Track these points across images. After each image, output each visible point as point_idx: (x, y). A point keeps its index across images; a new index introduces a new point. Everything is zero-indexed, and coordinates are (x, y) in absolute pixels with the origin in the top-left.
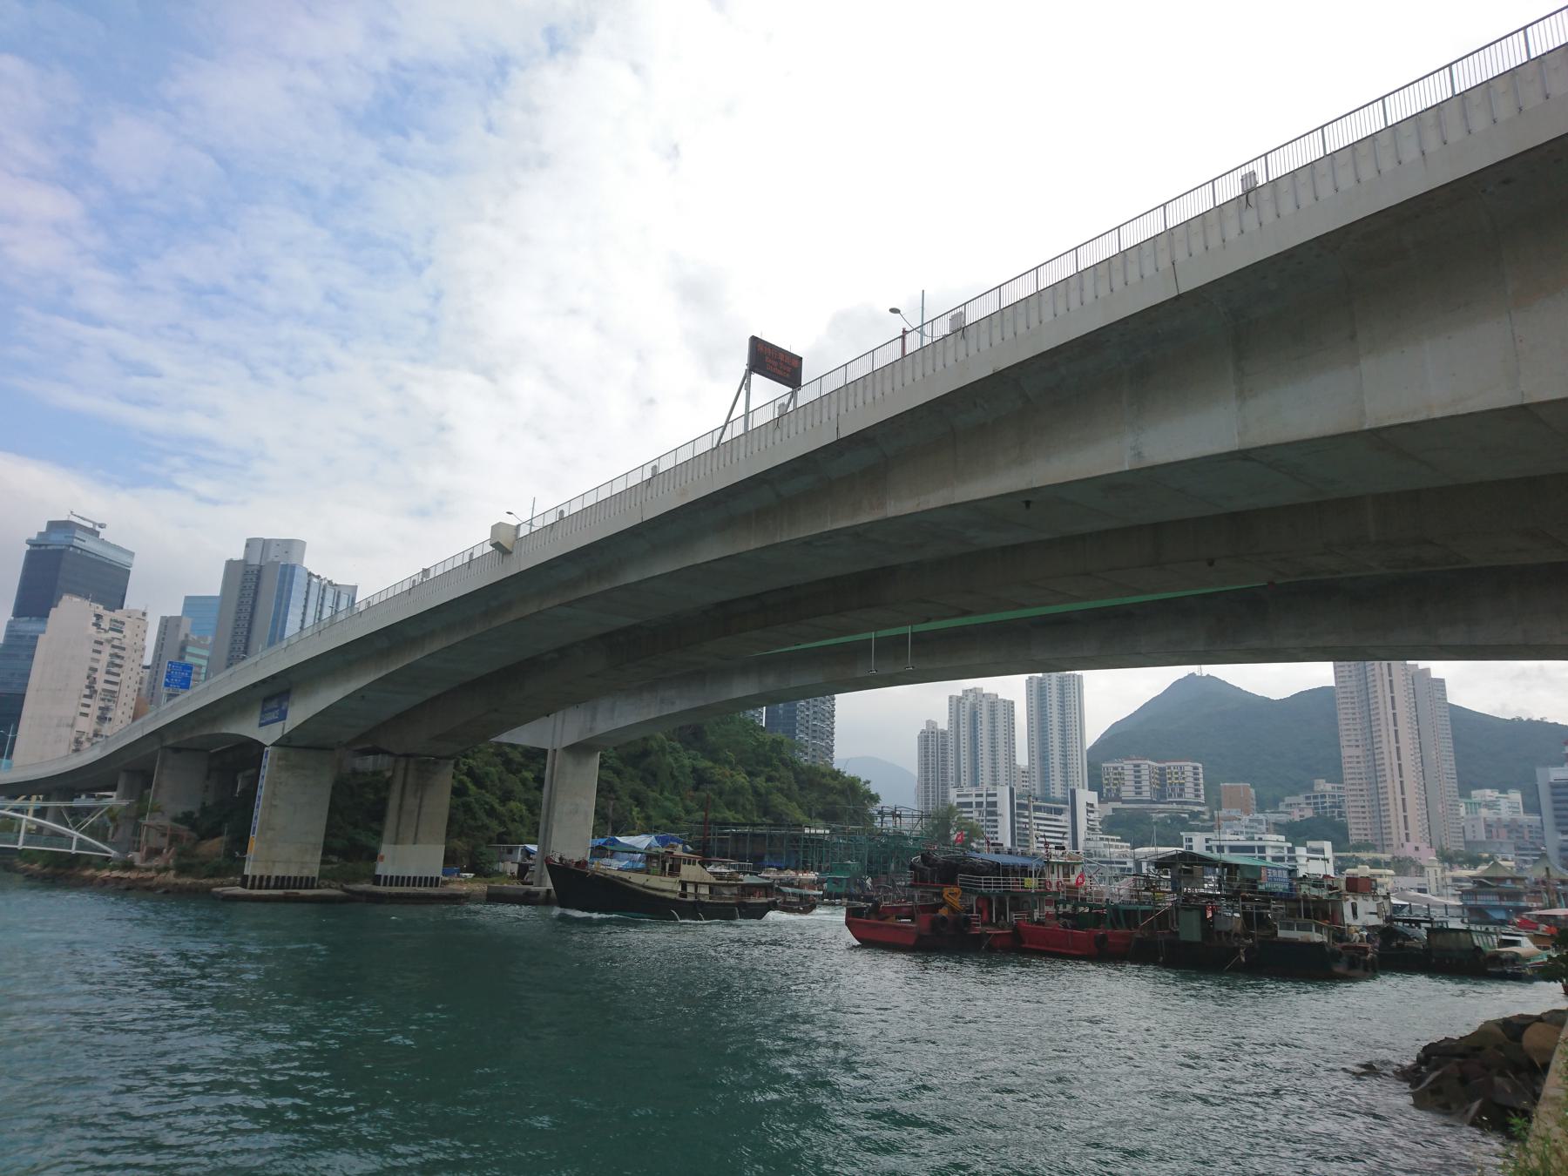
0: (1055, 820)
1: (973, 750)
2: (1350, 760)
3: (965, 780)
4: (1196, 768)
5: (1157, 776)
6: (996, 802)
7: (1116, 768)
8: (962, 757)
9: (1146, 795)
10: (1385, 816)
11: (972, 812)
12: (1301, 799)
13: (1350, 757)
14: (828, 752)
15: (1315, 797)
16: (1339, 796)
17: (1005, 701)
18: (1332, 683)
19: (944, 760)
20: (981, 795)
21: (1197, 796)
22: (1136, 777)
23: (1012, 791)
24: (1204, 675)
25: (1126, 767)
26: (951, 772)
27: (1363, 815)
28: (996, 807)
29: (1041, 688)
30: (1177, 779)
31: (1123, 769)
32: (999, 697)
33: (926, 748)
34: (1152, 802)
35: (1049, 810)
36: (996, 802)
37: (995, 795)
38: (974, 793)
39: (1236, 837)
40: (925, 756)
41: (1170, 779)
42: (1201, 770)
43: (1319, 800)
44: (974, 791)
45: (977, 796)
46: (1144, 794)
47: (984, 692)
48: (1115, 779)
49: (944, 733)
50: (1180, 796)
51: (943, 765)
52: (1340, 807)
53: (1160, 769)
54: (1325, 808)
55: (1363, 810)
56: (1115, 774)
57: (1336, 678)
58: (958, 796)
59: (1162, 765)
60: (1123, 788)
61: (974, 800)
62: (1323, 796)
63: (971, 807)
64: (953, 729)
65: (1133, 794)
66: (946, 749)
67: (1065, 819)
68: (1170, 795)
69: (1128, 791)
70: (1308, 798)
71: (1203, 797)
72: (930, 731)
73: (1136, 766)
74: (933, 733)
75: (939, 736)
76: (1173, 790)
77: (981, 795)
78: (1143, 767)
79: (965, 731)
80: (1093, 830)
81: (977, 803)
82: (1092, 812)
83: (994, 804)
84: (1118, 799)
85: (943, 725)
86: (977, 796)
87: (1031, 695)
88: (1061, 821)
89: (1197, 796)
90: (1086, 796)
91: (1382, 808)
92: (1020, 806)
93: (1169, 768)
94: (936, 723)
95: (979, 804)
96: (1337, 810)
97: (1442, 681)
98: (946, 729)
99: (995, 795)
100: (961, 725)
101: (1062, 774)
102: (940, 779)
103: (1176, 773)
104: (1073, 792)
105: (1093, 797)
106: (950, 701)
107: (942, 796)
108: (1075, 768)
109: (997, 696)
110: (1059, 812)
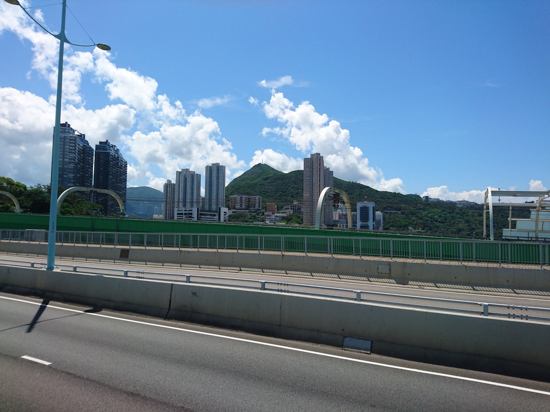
0: (213, 218)
1: (185, 187)
2: (306, 198)
3: (181, 191)
4: (259, 198)
5: (247, 201)
6: (192, 213)
7: (234, 198)
8: (180, 194)
9: (244, 207)
10: (314, 221)
11: (183, 217)
12: (289, 207)
13: (306, 197)
14: (124, 195)
15: (293, 206)
16: (300, 206)
17: (197, 174)
18: (302, 168)
19: (174, 195)
20: (187, 211)
21: (259, 207)
22: (242, 205)
23: (198, 209)
24: (263, 164)
25: (238, 198)
26: (176, 200)
27: (308, 215)
28: (192, 215)
29: (210, 190)
30: (253, 202)
31: (237, 198)
32: (196, 173)
33: (167, 190)
34: (245, 209)
35: (211, 215)
36: (192, 213)
37: (192, 210)
38: (184, 210)
39: (270, 223)
40: (166, 196)
41: (251, 202)
42: (261, 199)
43: (294, 207)
44: (184, 209)
45: (185, 211)
46: (243, 207)
47: (190, 170)
48: (234, 202)
49: (174, 185)
50: (254, 207)
51: (173, 199)
52: (300, 209)
53: (249, 198)
54: (296, 209)
55: (308, 213)
56: (234, 200)
57: (304, 168)
58: (178, 211)
59: (249, 197)
60: (236, 205)
61: (184, 212)
62: (296, 206)
63: (183, 215)
64: (177, 184)
65: (239, 207)
66: (174, 196)
67: (216, 217)
68: (251, 207)
69: (238, 206)
70: (291, 206)
71: (261, 207)
72: (169, 184)
73: (241, 197)
74: (170, 184)
75: (172, 185)
76: (252, 205)
77: (187, 211)
78: (243, 198)
79: (182, 185)
80: (226, 221)
81: (185, 213)
82: (226, 215)
83: (191, 214)
84: (234, 208)
85: (174, 182)
86: (185, 211)
87: (207, 172)
88: (215, 218)
89: (259, 207)
90: (224, 210)
91: (313, 220)
92: (201, 214)
93: (251, 198)
94: (171, 181)
95: (185, 214)
96: (299, 210)
97: (333, 172)
98: (175, 183)
99: (192, 210)
100: (181, 183)
101: (216, 201)
102: (171, 213)
103: (253, 200)
104: (220, 208)
105: (226, 210)
106: (177, 173)
107: (172, 208)
108: (221, 183)
109: (195, 172)
110: (214, 215)
